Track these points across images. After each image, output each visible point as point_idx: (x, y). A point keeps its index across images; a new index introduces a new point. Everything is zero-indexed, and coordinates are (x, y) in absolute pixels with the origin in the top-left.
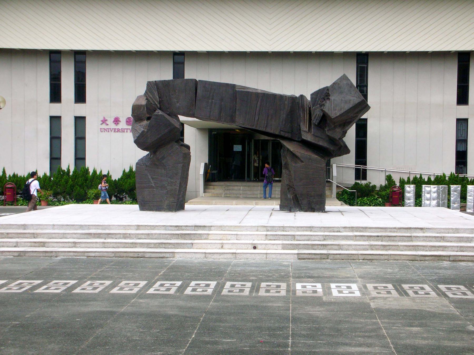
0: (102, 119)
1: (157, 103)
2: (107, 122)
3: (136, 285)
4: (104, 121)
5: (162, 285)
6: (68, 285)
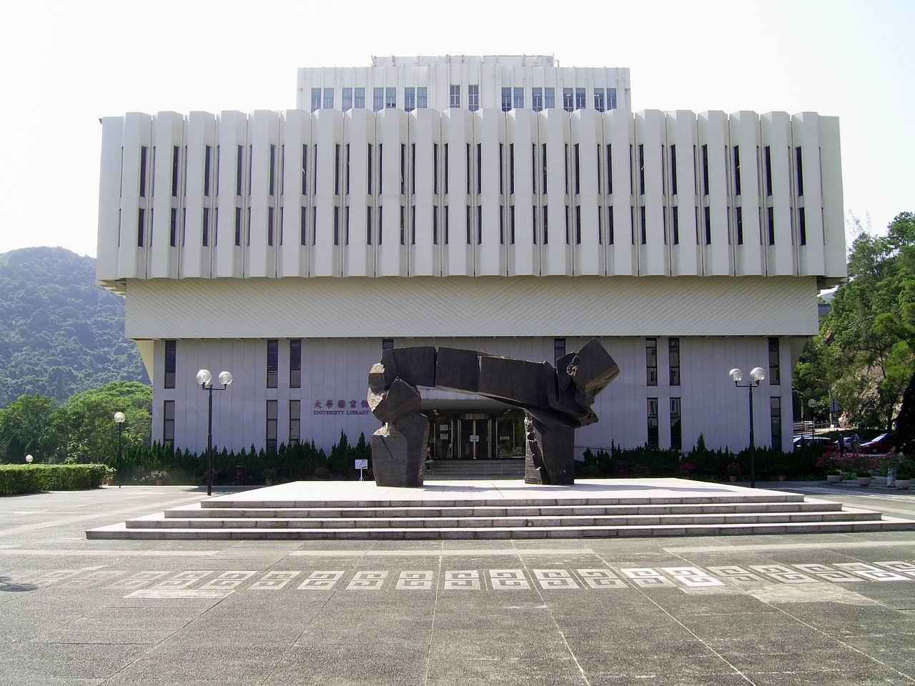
3: (332, 576)
4: (318, 404)
5: (364, 577)
6: (246, 578)
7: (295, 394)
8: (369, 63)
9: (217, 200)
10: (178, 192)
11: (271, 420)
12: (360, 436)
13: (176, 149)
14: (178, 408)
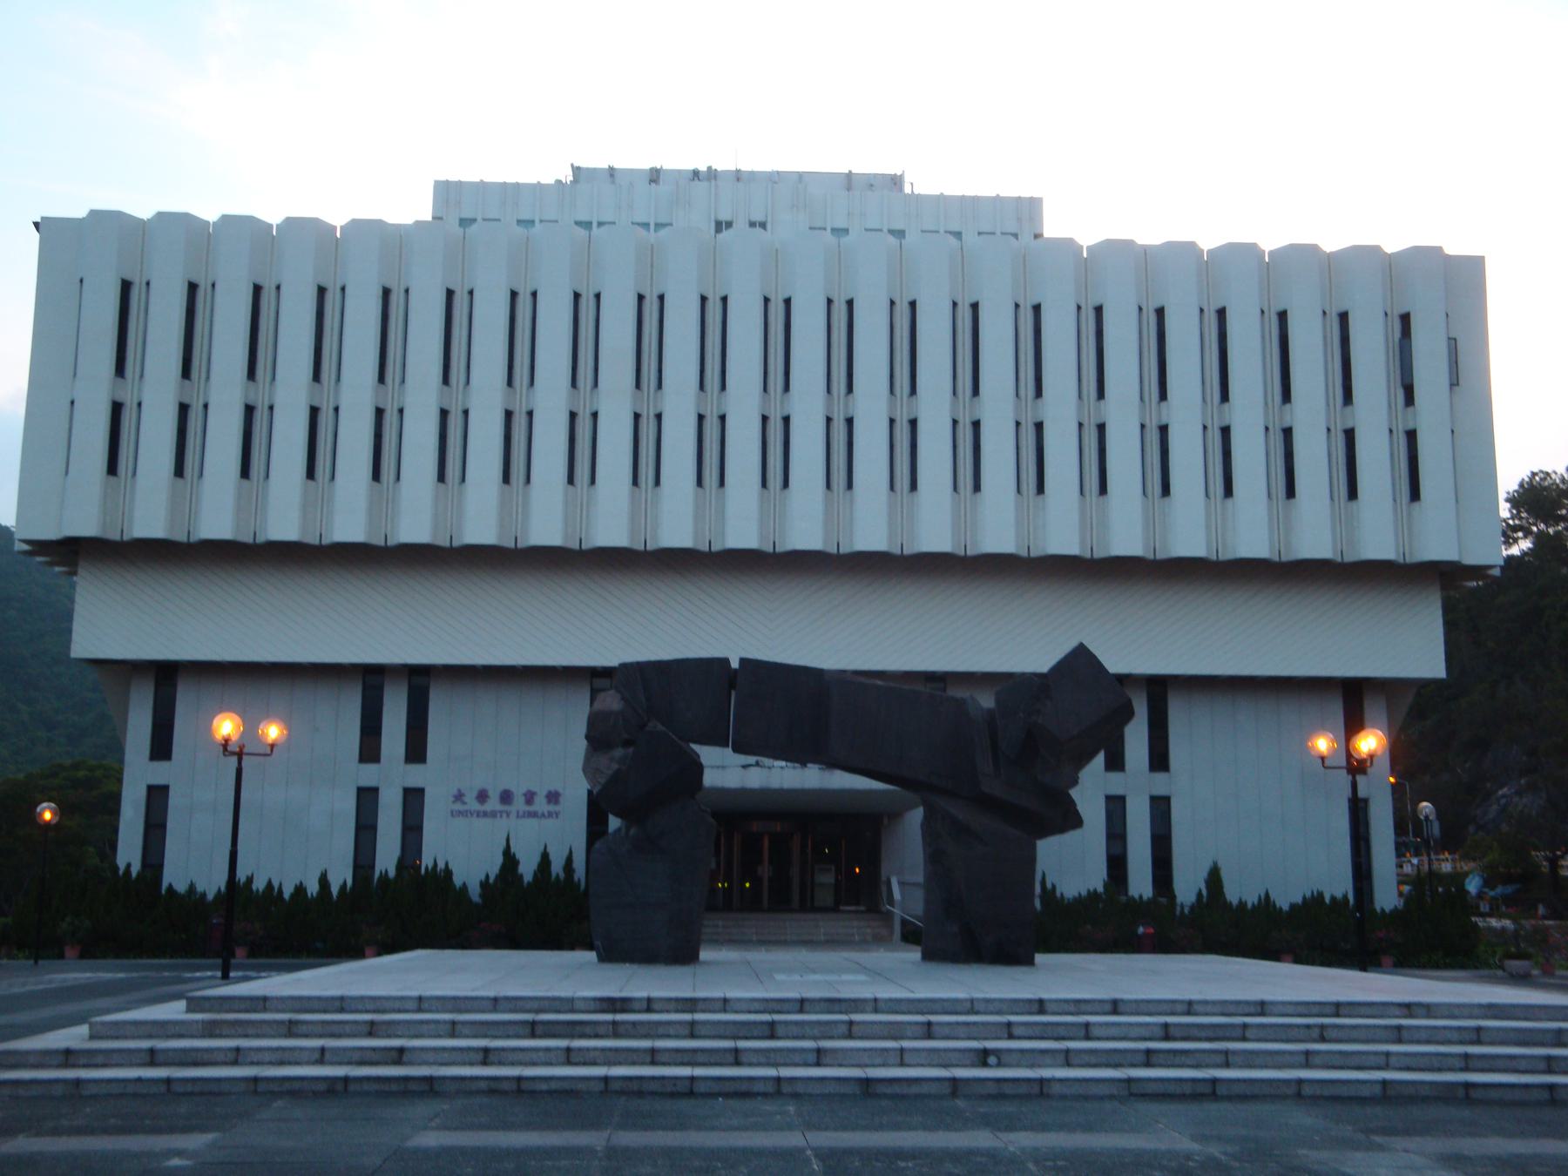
4: (459, 797)
7: (415, 776)
8: (567, 176)
9: (337, 392)
10: (194, 373)
11: (366, 829)
14: (174, 800)
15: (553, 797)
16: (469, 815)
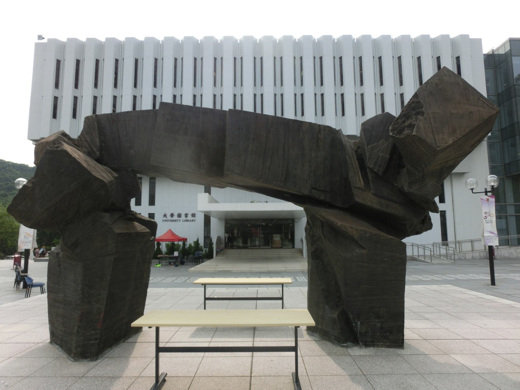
0: (164, 214)
1: (95, 150)
2: (166, 216)
4: (165, 216)
12: (197, 239)
13: (156, 60)
15: (193, 215)
16: (168, 221)
